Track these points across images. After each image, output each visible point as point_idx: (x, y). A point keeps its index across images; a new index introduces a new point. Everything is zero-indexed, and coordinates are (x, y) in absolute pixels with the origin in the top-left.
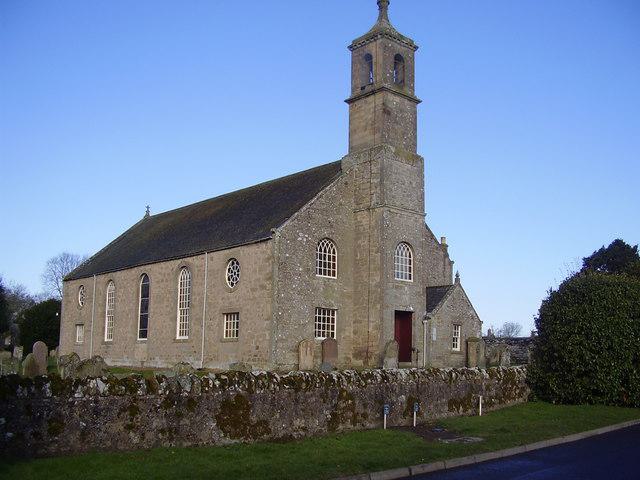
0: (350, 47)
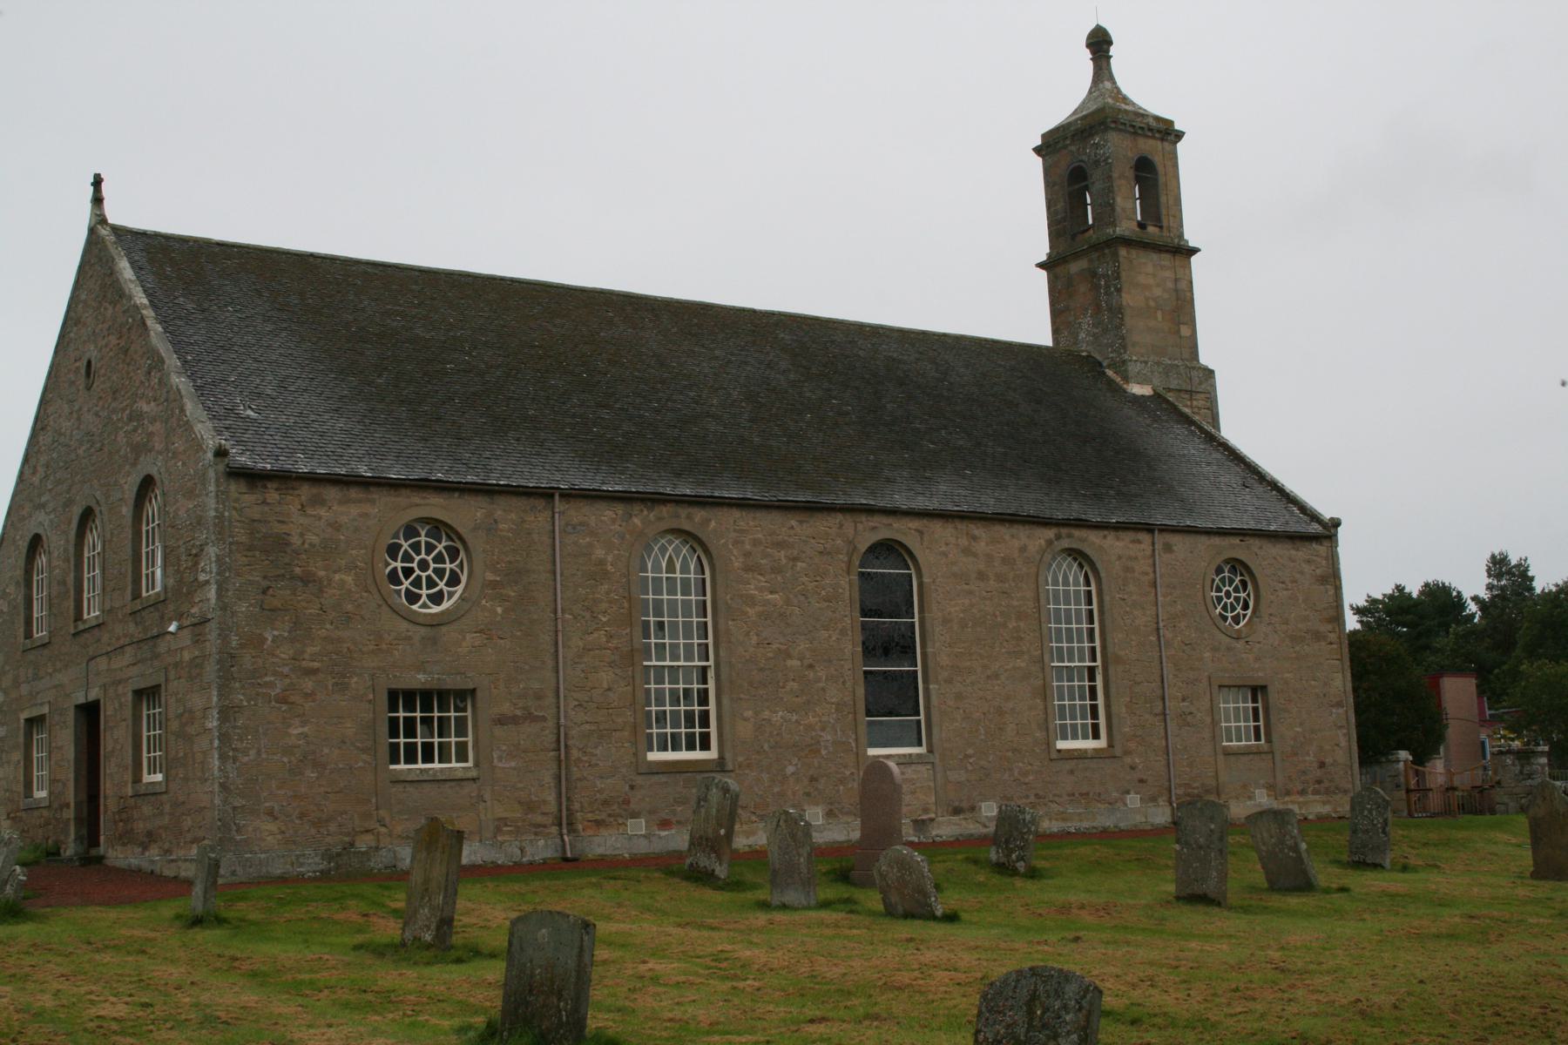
0: (1038, 150)
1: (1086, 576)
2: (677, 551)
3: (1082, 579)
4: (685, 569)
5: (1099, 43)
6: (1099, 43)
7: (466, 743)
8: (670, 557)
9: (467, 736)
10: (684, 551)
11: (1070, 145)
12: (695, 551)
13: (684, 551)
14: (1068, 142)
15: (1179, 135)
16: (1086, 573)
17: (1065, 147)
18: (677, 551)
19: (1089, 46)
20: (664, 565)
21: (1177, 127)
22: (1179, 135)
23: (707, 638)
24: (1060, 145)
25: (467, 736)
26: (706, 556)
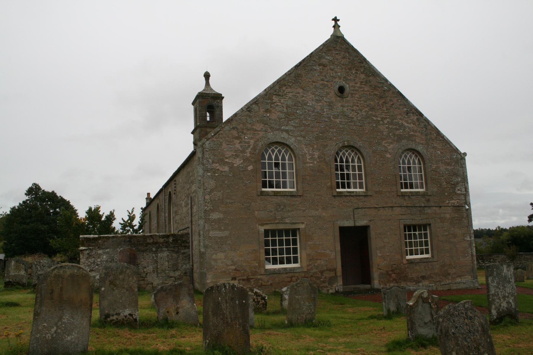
1: (359, 158)
2: (280, 151)
3: (417, 162)
4: (353, 161)
5: (207, 76)
6: (207, 76)
7: (428, 248)
8: (403, 159)
9: (428, 246)
10: (353, 154)
11: (210, 99)
12: (357, 154)
13: (353, 154)
14: (209, 98)
15: (223, 98)
16: (359, 157)
17: (208, 99)
18: (411, 157)
19: (204, 76)
20: (406, 162)
21: (223, 96)
22: (223, 98)
23: (293, 170)
24: (207, 98)
25: (428, 246)
26: (293, 153)
